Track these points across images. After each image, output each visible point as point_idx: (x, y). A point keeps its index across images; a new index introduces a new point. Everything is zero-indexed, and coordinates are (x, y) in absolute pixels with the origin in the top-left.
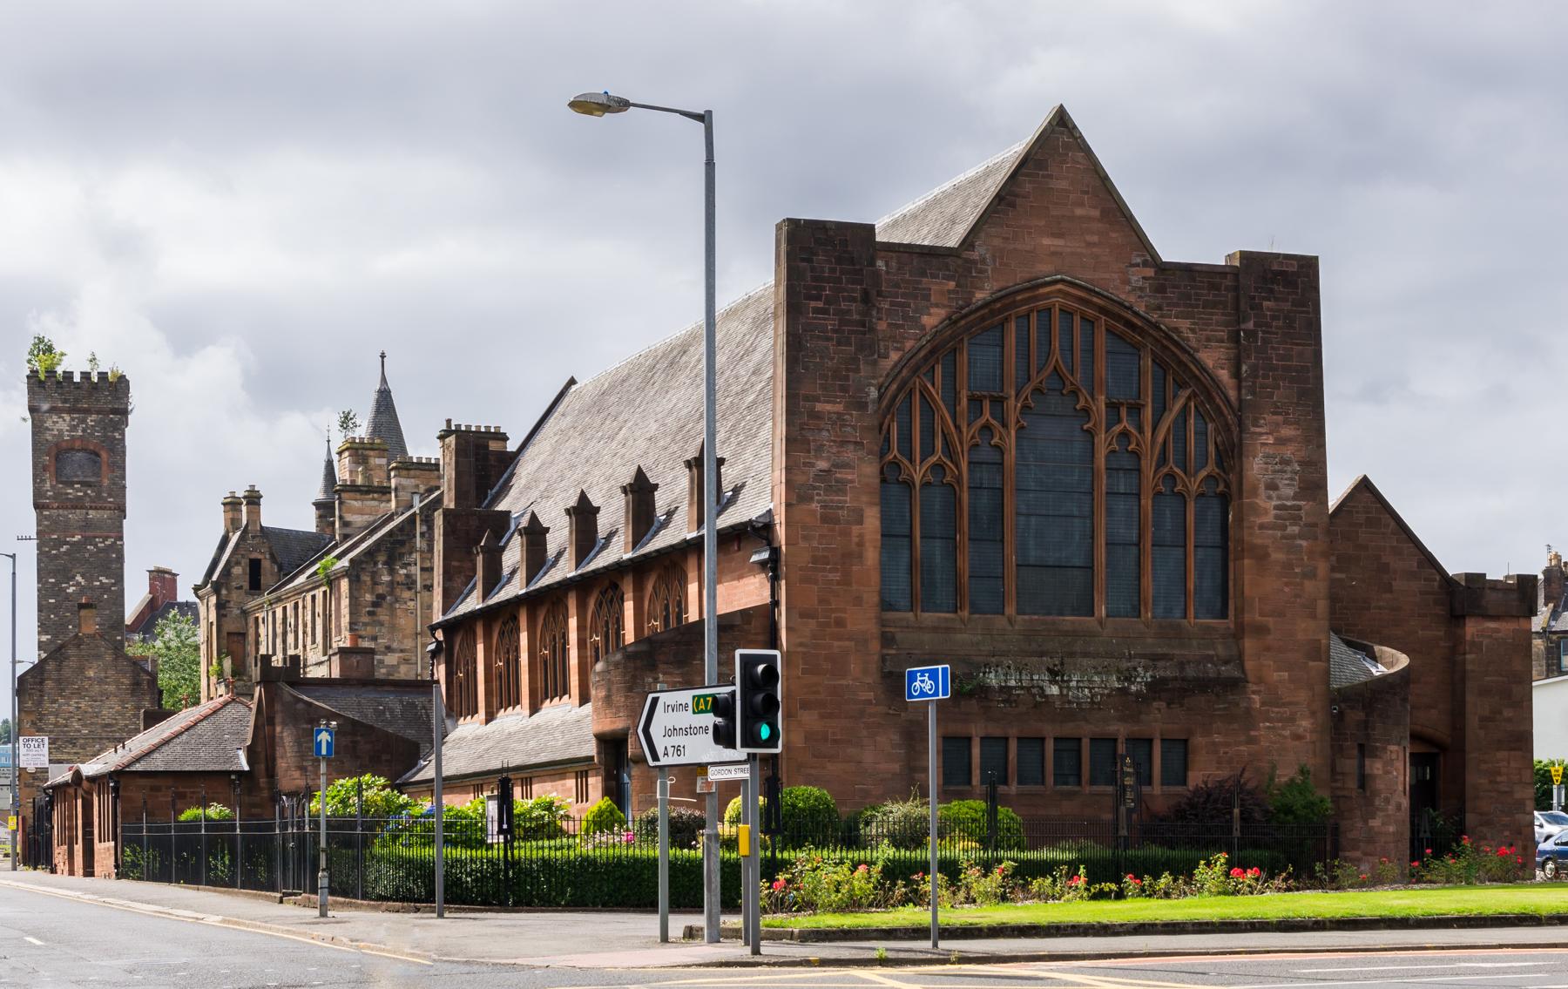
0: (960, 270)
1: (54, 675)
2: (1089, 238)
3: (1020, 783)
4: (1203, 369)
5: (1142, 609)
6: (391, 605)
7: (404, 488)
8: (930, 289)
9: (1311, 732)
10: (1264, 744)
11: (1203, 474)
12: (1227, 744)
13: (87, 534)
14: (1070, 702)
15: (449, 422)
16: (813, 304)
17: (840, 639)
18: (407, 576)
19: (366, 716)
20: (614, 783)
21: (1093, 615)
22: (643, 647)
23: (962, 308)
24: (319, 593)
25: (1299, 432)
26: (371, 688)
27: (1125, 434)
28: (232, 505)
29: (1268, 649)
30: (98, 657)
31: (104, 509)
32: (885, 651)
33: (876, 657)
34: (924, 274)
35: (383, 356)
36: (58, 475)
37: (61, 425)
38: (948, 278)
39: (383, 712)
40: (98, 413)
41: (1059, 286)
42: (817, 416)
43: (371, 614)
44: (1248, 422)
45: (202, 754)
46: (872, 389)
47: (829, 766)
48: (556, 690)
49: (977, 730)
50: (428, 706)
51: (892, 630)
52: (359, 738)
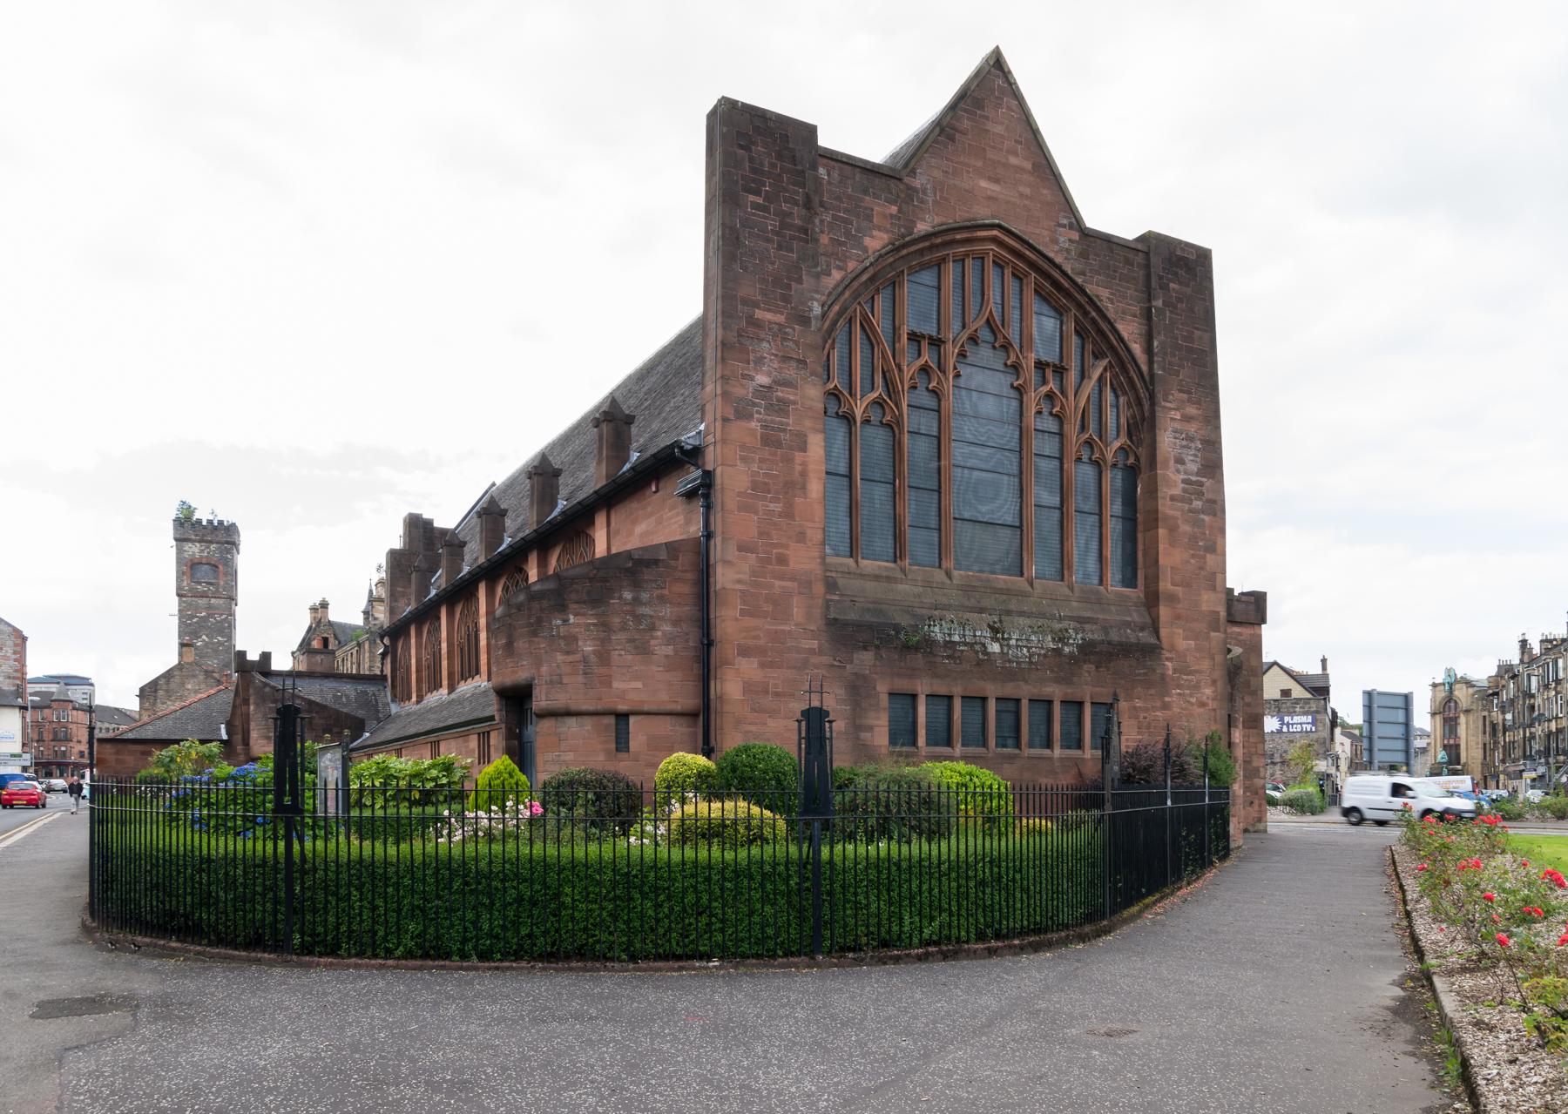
0: (903, 195)
1: (164, 687)
2: (1021, 189)
3: (963, 745)
4: (1121, 339)
5: (1066, 572)
8: (872, 210)
9: (1213, 700)
10: (1176, 710)
11: (1117, 445)
12: (1146, 710)
14: (1010, 661)
16: (751, 198)
17: (781, 578)
19: (326, 700)
20: (516, 742)
21: (1022, 575)
22: (551, 585)
23: (903, 237)
24: (354, 651)
25: (1200, 412)
27: (1050, 396)
28: (314, 609)
29: (1178, 617)
30: (194, 676)
32: (828, 597)
33: (820, 601)
34: (866, 192)
36: (192, 576)
37: (194, 549)
38: (892, 202)
39: (341, 697)
40: (217, 543)
41: (995, 233)
42: (758, 324)
44: (1159, 396)
46: (815, 304)
47: (771, 722)
48: (470, 672)
49: (923, 687)
50: (377, 693)
51: (834, 575)
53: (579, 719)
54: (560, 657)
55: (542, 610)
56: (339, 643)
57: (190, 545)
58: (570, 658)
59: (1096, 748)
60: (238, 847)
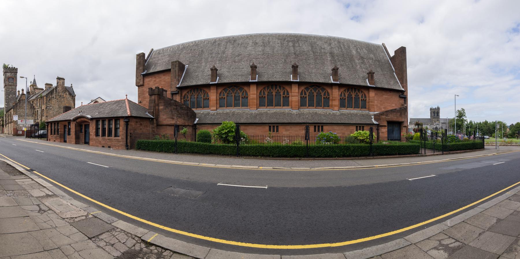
18: (53, 96)
37: (9, 74)
40: (14, 73)
43: (49, 101)
59: (327, 99)
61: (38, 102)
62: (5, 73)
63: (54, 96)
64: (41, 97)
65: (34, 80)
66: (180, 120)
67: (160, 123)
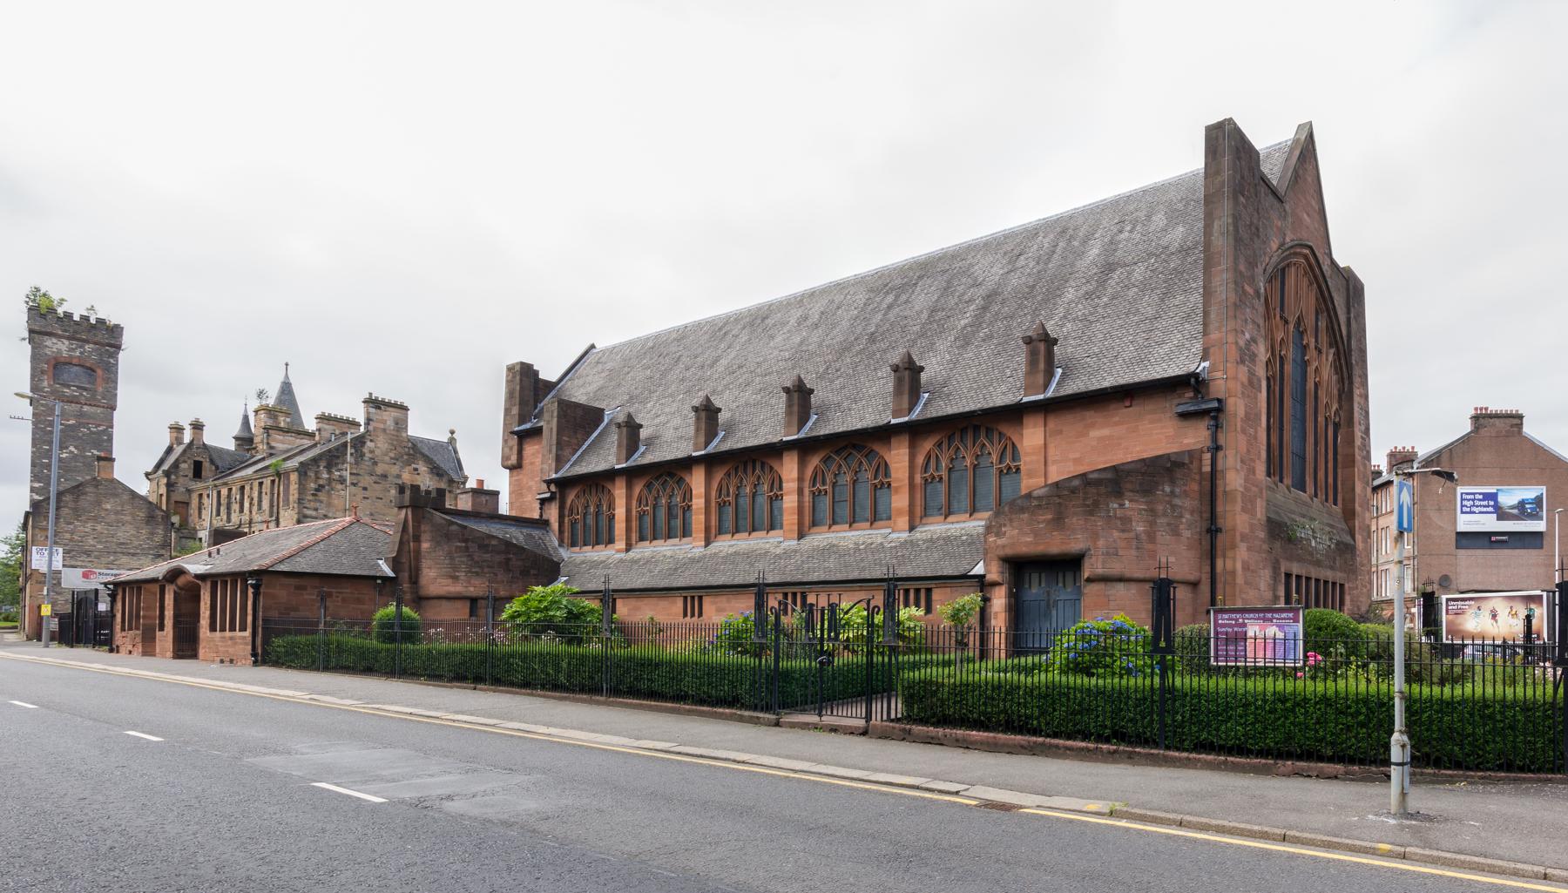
1: (71, 505)
6: (328, 491)
7: (325, 430)
13: (81, 421)
15: (371, 394)
18: (340, 476)
26: (496, 521)
31: (98, 406)
35: (287, 365)
40: (95, 343)
45: (345, 561)
52: (511, 556)
53: (1127, 584)
54: (1116, 534)
55: (1099, 495)
56: (217, 468)
57: (54, 340)
58: (1126, 535)
60: (1538, 693)
61: (264, 494)
62: (36, 334)
63: (347, 474)
64: (278, 474)
65: (286, 389)
66: (476, 581)
67: (423, 593)
